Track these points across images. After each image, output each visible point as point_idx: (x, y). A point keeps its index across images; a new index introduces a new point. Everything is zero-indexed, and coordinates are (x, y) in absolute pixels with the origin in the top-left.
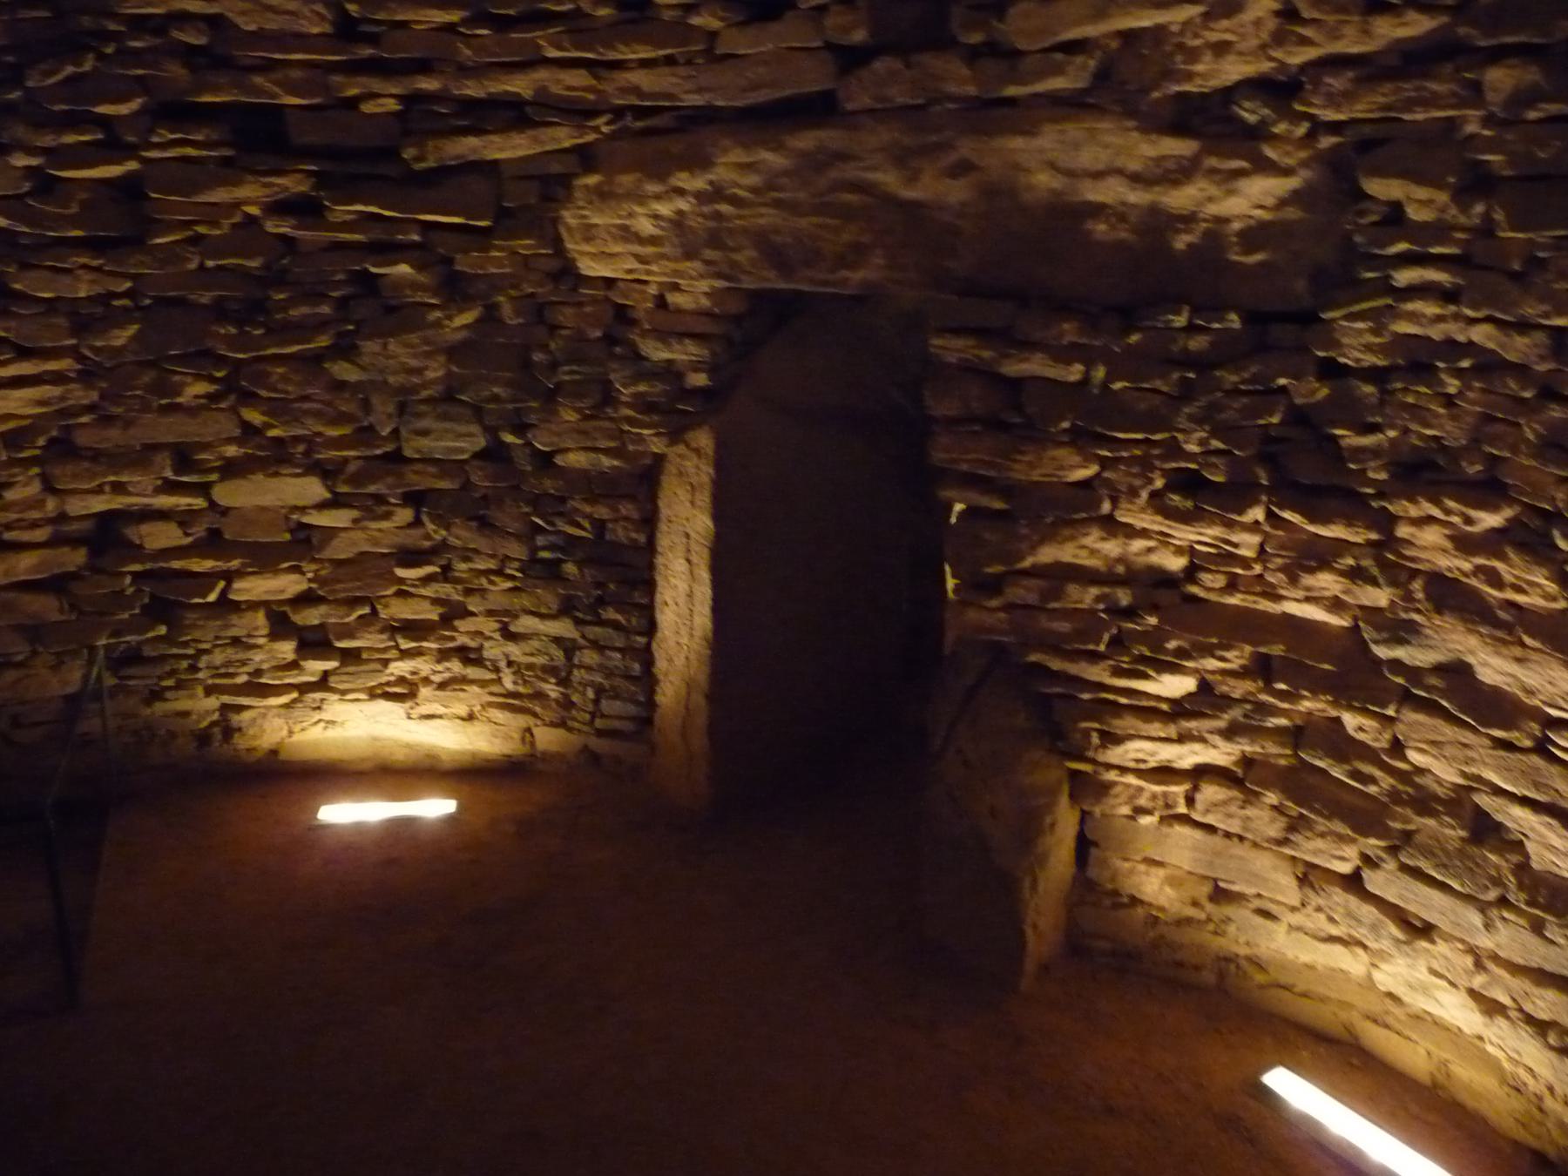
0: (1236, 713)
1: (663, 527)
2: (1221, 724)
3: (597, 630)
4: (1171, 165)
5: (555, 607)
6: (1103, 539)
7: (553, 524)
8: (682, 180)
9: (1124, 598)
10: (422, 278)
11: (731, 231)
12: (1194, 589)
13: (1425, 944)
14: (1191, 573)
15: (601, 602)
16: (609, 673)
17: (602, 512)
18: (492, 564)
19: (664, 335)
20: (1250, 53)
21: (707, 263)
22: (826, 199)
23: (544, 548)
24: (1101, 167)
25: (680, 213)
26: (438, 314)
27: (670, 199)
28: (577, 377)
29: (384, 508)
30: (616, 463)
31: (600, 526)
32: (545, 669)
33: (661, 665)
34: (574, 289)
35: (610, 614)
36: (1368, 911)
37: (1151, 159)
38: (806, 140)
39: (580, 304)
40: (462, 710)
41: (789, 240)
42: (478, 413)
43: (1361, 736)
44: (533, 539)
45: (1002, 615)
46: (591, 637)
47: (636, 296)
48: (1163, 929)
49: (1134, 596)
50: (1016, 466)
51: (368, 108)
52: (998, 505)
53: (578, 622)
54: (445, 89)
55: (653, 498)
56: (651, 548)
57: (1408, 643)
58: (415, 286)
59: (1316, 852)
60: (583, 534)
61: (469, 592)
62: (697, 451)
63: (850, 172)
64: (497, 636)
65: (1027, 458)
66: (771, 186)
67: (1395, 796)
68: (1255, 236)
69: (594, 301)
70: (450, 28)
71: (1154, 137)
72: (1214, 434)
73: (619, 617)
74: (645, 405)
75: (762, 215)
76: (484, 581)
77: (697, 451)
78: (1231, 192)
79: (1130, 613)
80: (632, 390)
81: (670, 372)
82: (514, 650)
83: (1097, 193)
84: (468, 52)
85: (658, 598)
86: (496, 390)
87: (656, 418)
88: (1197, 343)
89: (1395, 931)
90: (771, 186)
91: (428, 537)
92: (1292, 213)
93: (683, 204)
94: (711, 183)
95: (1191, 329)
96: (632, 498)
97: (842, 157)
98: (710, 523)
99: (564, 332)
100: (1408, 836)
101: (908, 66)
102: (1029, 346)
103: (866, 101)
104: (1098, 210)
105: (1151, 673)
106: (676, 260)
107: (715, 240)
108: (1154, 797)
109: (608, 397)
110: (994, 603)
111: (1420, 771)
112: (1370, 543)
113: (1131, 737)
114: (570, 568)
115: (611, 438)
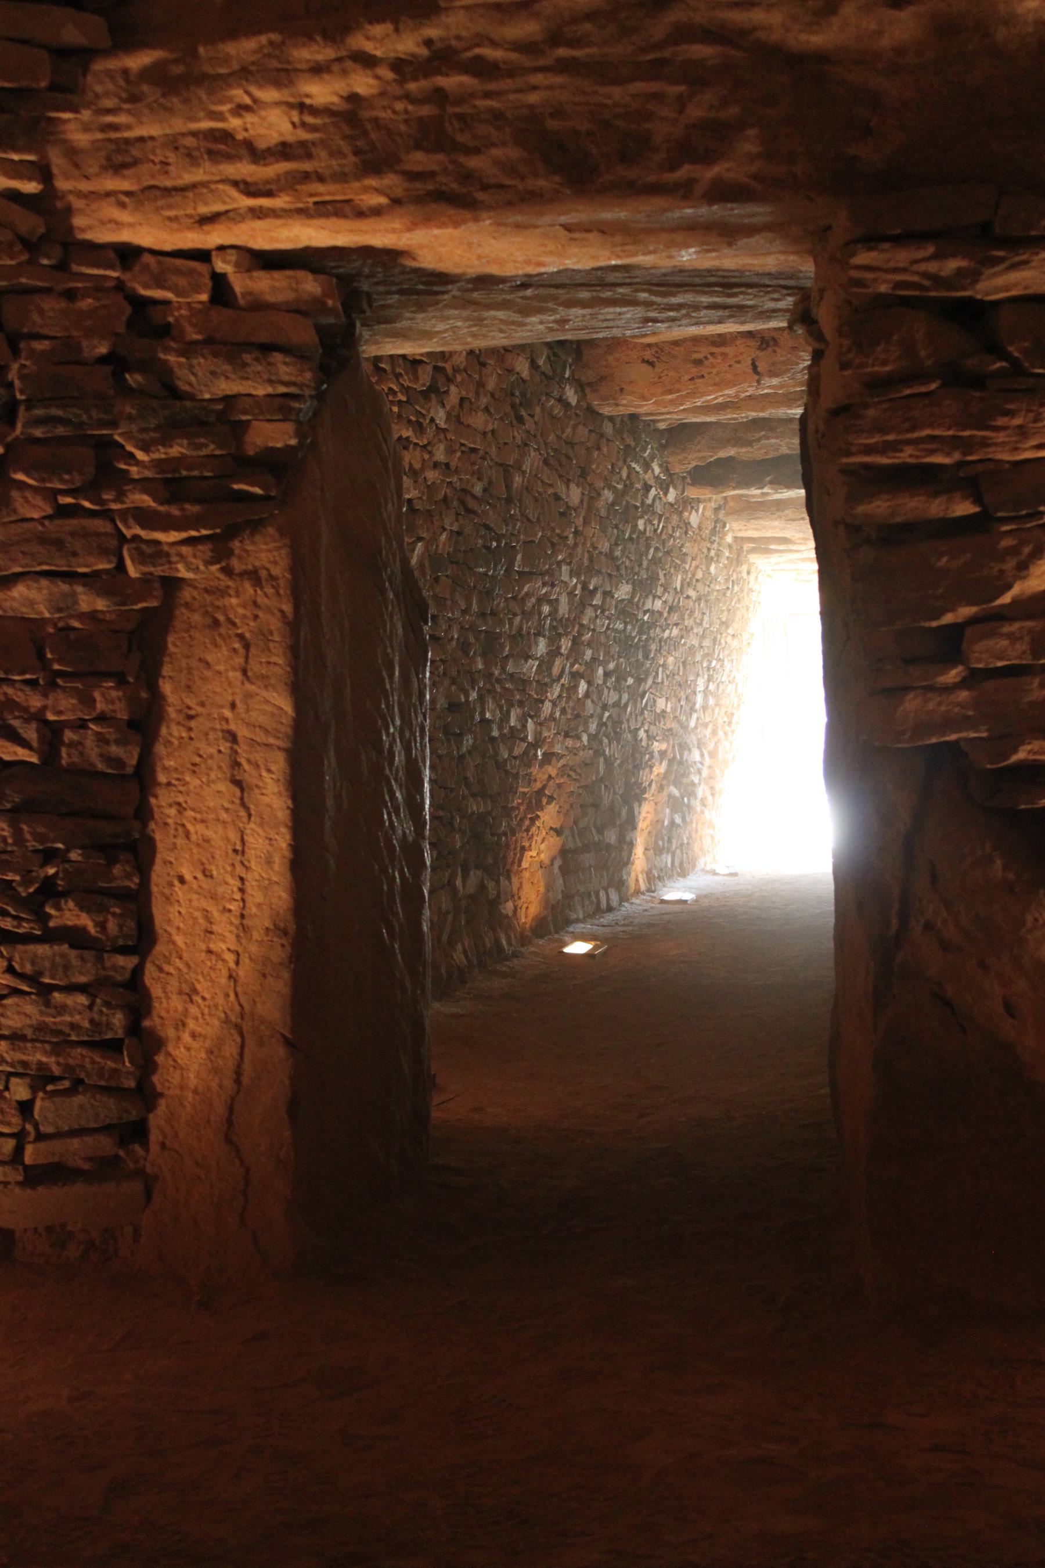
1: (172, 731)
3: (43, 950)
8: (379, 39)
15: (49, 891)
16: (60, 1043)
17: (62, 706)
19: (232, 350)
21: (412, 176)
22: (667, 53)
25: (353, 98)
27: (345, 73)
28: (61, 431)
31: (52, 734)
33: (166, 1003)
34: (62, 267)
35: (69, 915)
39: (70, 295)
45: (963, 695)
46: (28, 969)
47: (182, 282)
50: (1001, 437)
52: (964, 508)
55: (150, 676)
56: (143, 777)
60: (22, 754)
62: (254, 576)
65: (1017, 421)
66: (555, 39)
69: (98, 287)
73: (86, 921)
74: (171, 485)
75: (535, 88)
77: (254, 576)
80: (160, 453)
81: (226, 419)
85: (159, 874)
87: (193, 509)
90: (555, 39)
93: (363, 84)
94: (428, 43)
98: (286, 705)
106: (342, 177)
107: (430, 135)
109: (105, 470)
110: (954, 675)
115: (104, 552)
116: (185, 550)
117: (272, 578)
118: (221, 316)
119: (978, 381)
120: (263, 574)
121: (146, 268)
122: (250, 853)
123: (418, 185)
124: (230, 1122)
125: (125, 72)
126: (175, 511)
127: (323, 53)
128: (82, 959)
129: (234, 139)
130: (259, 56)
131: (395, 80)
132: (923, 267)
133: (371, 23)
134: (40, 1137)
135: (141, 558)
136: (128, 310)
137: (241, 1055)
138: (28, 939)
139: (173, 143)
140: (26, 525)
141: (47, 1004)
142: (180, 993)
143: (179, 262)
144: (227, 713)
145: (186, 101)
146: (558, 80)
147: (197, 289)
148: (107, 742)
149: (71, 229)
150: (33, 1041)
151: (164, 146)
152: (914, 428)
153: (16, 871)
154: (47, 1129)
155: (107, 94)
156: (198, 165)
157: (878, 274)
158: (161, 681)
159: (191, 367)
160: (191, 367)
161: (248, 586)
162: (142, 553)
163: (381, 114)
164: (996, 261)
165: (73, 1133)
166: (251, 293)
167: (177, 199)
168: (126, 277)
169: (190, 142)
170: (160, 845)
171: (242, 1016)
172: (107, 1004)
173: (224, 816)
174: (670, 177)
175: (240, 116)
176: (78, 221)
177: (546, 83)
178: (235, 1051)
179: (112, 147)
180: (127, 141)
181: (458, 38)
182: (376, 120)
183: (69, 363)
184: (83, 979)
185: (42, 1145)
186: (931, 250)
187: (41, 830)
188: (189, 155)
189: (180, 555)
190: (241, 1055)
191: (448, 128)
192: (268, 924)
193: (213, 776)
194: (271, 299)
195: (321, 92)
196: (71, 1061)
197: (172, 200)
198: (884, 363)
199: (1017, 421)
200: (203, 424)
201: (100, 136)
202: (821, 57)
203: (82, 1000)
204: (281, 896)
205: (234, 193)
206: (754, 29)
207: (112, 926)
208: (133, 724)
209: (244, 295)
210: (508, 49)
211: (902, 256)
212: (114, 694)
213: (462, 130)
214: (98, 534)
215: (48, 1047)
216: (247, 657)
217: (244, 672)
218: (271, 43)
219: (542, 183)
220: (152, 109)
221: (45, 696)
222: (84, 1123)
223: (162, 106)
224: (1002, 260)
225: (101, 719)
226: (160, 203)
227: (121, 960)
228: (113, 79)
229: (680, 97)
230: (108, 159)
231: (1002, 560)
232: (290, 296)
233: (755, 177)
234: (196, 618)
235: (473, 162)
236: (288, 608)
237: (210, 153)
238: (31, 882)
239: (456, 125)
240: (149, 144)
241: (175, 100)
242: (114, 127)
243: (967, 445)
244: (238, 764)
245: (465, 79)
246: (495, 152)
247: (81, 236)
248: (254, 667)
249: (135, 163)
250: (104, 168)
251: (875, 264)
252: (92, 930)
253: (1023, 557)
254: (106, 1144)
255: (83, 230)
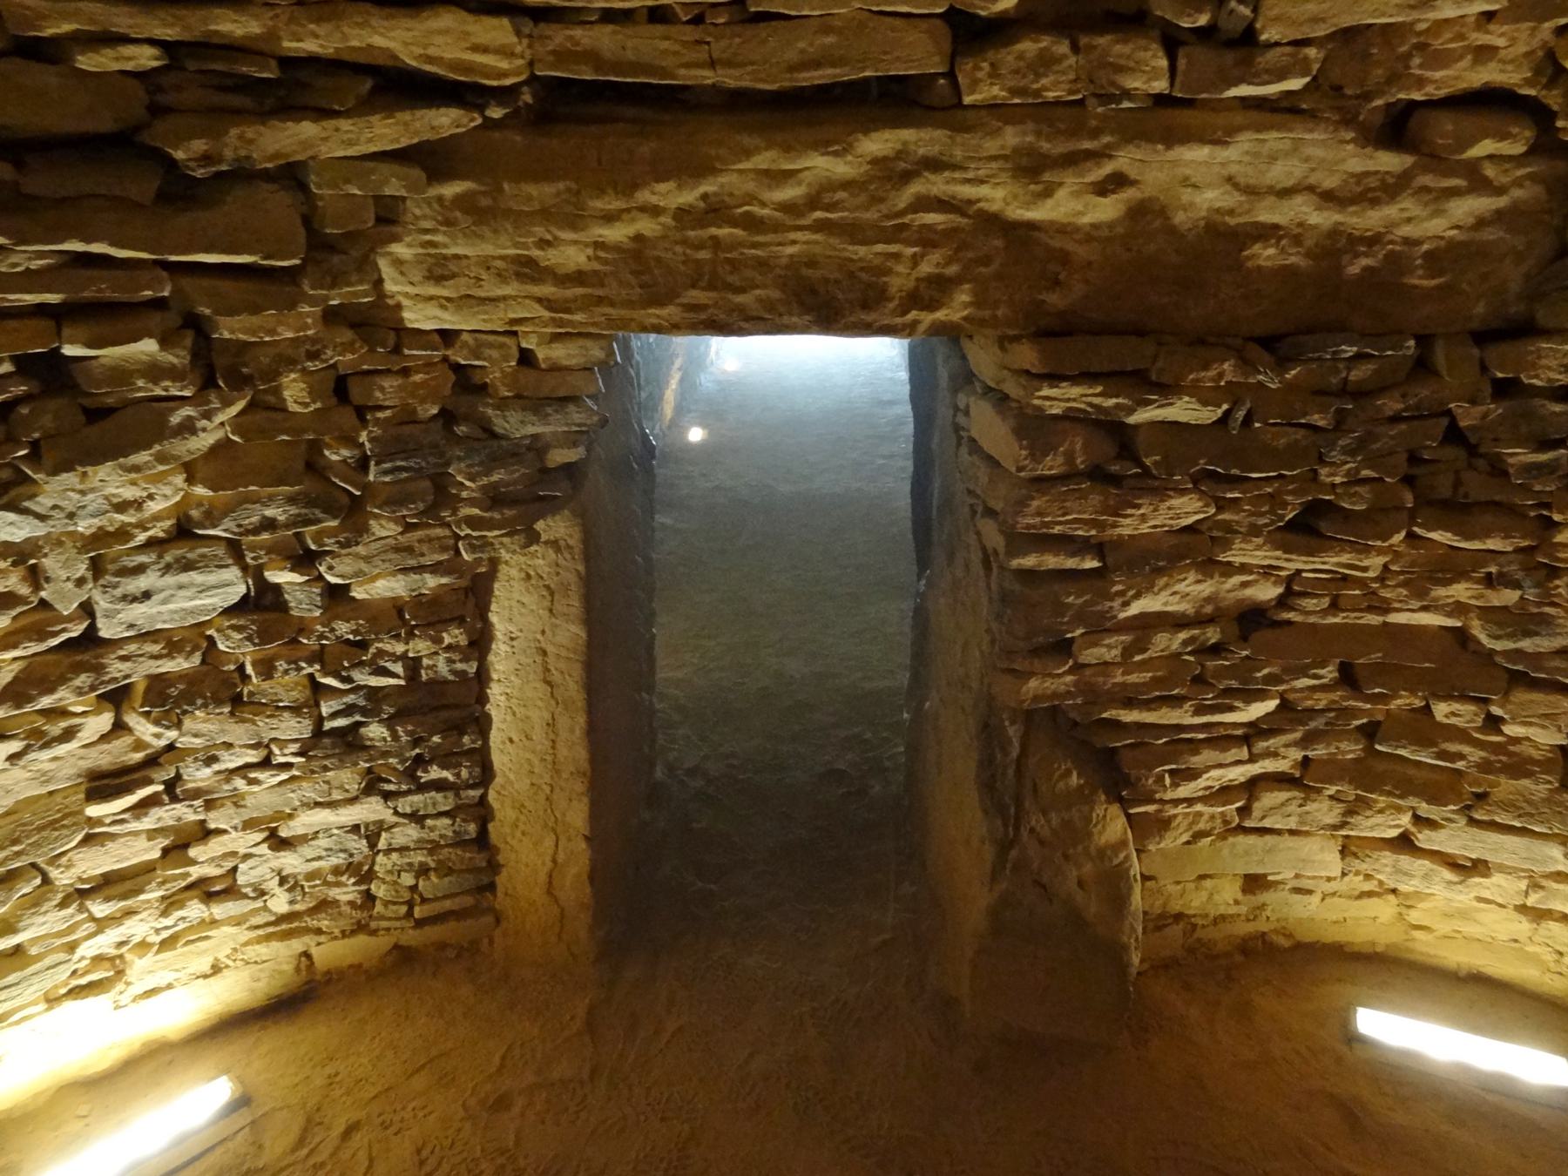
0: (1317, 723)
2: (1298, 735)
3: (417, 798)
4: (1373, 182)
6: (1199, 582)
7: (348, 680)
9: (1213, 635)
10: (169, 358)
11: (734, 265)
12: (1291, 616)
13: (1477, 880)
15: (419, 761)
18: (253, 757)
19: (537, 404)
20: (1512, 61)
22: (906, 220)
23: (334, 715)
24: (1290, 183)
26: (188, 411)
29: (63, 724)
30: (444, 580)
31: (413, 665)
32: (337, 871)
34: (397, 350)
35: (435, 773)
36: (1425, 864)
37: (1353, 175)
38: (878, 144)
39: (405, 372)
40: (204, 965)
42: (235, 549)
43: (1453, 720)
44: (317, 705)
46: (408, 810)
47: (495, 354)
50: (1128, 521)
51: (87, 62)
52: (1091, 564)
53: (387, 796)
57: (1537, 634)
58: (154, 371)
59: (1372, 828)
61: (209, 805)
63: (936, 185)
64: (264, 849)
67: (1485, 767)
68: (1443, 257)
69: (429, 365)
71: (1369, 150)
73: (446, 774)
74: (494, 498)
75: (794, 242)
76: (239, 783)
78: (1438, 213)
82: (291, 862)
83: (1268, 213)
86: (269, 512)
89: (1448, 875)
91: (139, 745)
92: (1490, 234)
93: (647, 226)
95: (1359, 357)
96: (460, 621)
97: (934, 165)
100: (1481, 797)
102: (1168, 390)
103: (994, 92)
104: (1268, 232)
106: (630, 304)
108: (1212, 817)
109: (442, 495)
111: (1516, 740)
112: (1518, 550)
114: (375, 731)
115: (444, 549)
116: (505, 540)
117: (569, 547)
118: (528, 376)
120: (562, 543)
121: (465, 344)
123: (692, 315)
124: (550, 883)
125: (440, 199)
126: (497, 516)
127: (617, 204)
132: (1089, 399)
133: (657, 181)
134: (424, 900)
135: (472, 548)
136: (453, 377)
138: (409, 792)
139: (485, 263)
141: (423, 827)
143: (491, 338)
145: (495, 231)
147: (506, 359)
148: (454, 662)
149: (402, 320)
151: (477, 264)
152: (1064, 515)
154: (428, 895)
155: (425, 217)
159: (504, 417)
160: (504, 417)
164: (1148, 403)
165: (445, 897)
168: (449, 352)
169: (499, 263)
172: (464, 820)
174: (898, 320)
176: (406, 315)
177: (805, 239)
178: (552, 844)
180: (445, 257)
182: (658, 260)
186: (1099, 389)
187: (410, 728)
188: (499, 275)
191: (720, 269)
194: (565, 363)
195: (616, 233)
198: (1051, 468)
200: (514, 455)
201: (421, 251)
202: (1032, 226)
203: (447, 821)
204: (582, 754)
205: (537, 306)
206: (979, 200)
207: (464, 773)
211: (1075, 391)
213: (731, 273)
214: (439, 538)
217: (551, 611)
218: (569, 190)
219: (795, 319)
220: (465, 235)
223: (474, 233)
224: (1155, 401)
225: (449, 648)
227: (472, 793)
228: (429, 205)
230: (429, 270)
231: (1112, 600)
232: (582, 360)
233: (965, 319)
235: (740, 299)
236: (581, 568)
239: (728, 268)
240: (465, 262)
246: (758, 292)
248: (558, 607)
249: (453, 276)
250: (428, 278)
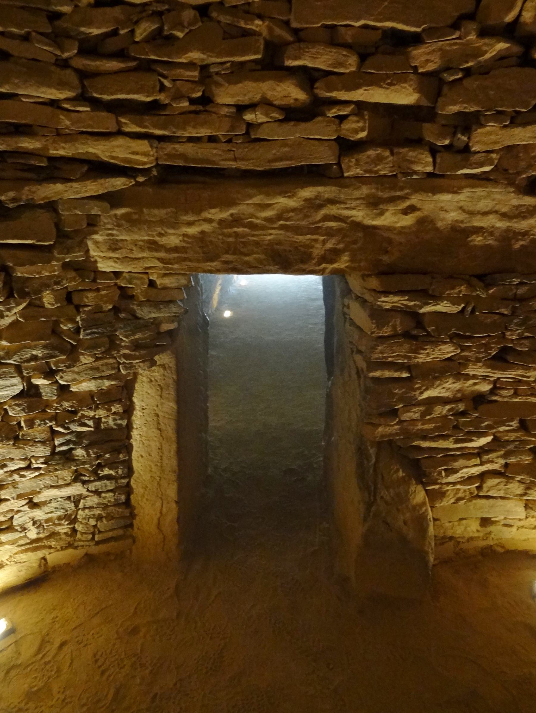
0: (511, 447)
2: (502, 453)
3: (98, 484)
4: (524, 209)
5: (69, 479)
6: (454, 383)
9: (461, 407)
14: (492, 392)
15: (100, 466)
18: (23, 464)
22: (320, 225)
23: (61, 445)
24: (487, 209)
30: (113, 383)
32: (59, 518)
34: (94, 281)
35: (107, 471)
38: (308, 193)
39: (98, 290)
41: (288, 248)
44: (53, 440)
46: (94, 489)
47: (138, 282)
48: (462, 546)
49: (466, 406)
52: (405, 375)
53: (84, 483)
54: (45, 148)
64: (26, 508)
65: (427, 352)
69: (108, 287)
70: (54, 103)
71: (520, 196)
72: (527, 330)
73: (111, 472)
74: (136, 346)
75: (271, 234)
79: (463, 414)
83: (478, 222)
84: (68, 123)
86: (35, 353)
88: (521, 291)
93: (206, 227)
96: (119, 401)
97: (332, 202)
99: (86, 309)
101: (392, 154)
104: (478, 230)
105: (474, 438)
106: (198, 261)
108: (465, 491)
109: (113, 344)
113: (462, 468)
114: (79, 452)
115: (113, 368)
117: (170, 367)
118: (152, 292)
119: (415, 338)
120: (166, 366)
121: (125, 278)
122: (164, 449)
123: (225, 265)
125: (115, 215)
126: (137, 354)
128: (111, 483)
129: (158, 244)
130: (167, 216)
131: (219, 228)
134: (100, 532)
135: (126, 368)
137: (162, 506)
139: (135, 243)
140: (85, 365)
141: (100, 497)
142: (142, 488)
144: (156, 408)
146: (281, 232)
147: (143, 284)
149: (97, 267)
150: (96, 508)
151: (131, 243)
153: (88, 464)
155: (108, 223)
156: (144, 252)
157: (387, 304)
158: (133, 398)
159: (142, 310)
161: (161, 369)
162: (125, 366)
163: (213, 239)
165: (110, 530)
166: (162, 284)
167: (136, 262)
169: (141, 243)
170: (134, 446)
171: (162, 495)
172: (119, 494)
173: (155, 439)
174: (317, 268)
175: (160, 237)
176: (99, 265)
177: (275, 233)
179: (111, 242)
180: (117, 240)
181: (243, 214)
182: (211, 242)
183: (98, 312)
184: (111, 488)
185: (100, 535)
186: (407, 298)
187: (95, 451)
188: (141, 248)
189: (139, 366)
190: (162, 506)
192: (169, 469)
193: (151, 427)
196: (108, 511)
197: (135, 262)
198: (386, 332)
199: (427, 352)
201: (106, 238)
202: (375, 227)
203: (111, 494)
206: (352, 217)
207: (120, 472)
208: (125, 412)
209: (160, 285)
210: (262, 220)
211: (396, 299)
212: (118, 406)
213: (243, 248)
214: (111, 364)
215: (101, 509)
216: (161, 392)
217: (161, 396)
219: (271, 267)
221: (95, 412)
222: (114, 527)
224: (431, 303)
226: (130, 263)
227: (123, 481)
229: (324, 240)
230: (110, 246)
231: (415, 391)
232: (176, 284)
234: (145, 379)
236: (175, 377)
237: (149, 248)
238: (93, 466)
240: (125, 243)
241: (135, 228)
242: (112, 235)
243: (409, 358)
244: (159, 423)
245: (246, 230)
247: (101, 270)
249: (120, 248)
251: (386, 300)
252: (114, 474)
253: (421, 391)
254: (121, 532)
255: (101, 268)
